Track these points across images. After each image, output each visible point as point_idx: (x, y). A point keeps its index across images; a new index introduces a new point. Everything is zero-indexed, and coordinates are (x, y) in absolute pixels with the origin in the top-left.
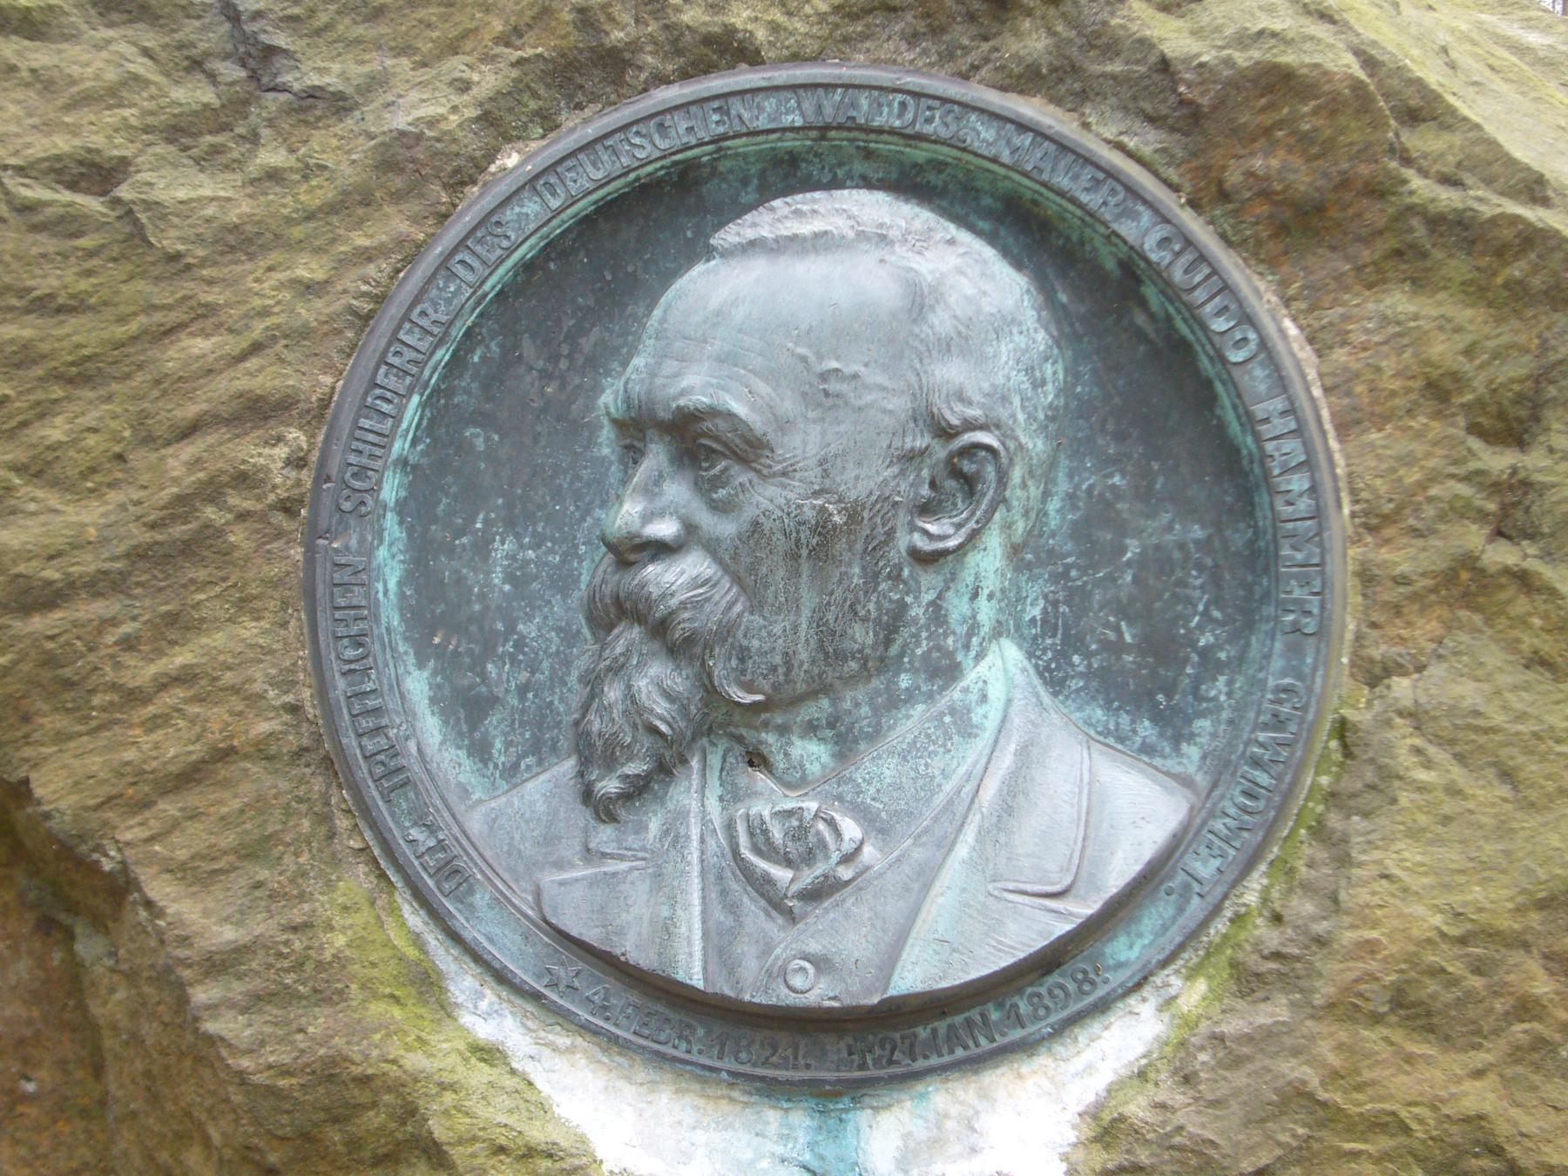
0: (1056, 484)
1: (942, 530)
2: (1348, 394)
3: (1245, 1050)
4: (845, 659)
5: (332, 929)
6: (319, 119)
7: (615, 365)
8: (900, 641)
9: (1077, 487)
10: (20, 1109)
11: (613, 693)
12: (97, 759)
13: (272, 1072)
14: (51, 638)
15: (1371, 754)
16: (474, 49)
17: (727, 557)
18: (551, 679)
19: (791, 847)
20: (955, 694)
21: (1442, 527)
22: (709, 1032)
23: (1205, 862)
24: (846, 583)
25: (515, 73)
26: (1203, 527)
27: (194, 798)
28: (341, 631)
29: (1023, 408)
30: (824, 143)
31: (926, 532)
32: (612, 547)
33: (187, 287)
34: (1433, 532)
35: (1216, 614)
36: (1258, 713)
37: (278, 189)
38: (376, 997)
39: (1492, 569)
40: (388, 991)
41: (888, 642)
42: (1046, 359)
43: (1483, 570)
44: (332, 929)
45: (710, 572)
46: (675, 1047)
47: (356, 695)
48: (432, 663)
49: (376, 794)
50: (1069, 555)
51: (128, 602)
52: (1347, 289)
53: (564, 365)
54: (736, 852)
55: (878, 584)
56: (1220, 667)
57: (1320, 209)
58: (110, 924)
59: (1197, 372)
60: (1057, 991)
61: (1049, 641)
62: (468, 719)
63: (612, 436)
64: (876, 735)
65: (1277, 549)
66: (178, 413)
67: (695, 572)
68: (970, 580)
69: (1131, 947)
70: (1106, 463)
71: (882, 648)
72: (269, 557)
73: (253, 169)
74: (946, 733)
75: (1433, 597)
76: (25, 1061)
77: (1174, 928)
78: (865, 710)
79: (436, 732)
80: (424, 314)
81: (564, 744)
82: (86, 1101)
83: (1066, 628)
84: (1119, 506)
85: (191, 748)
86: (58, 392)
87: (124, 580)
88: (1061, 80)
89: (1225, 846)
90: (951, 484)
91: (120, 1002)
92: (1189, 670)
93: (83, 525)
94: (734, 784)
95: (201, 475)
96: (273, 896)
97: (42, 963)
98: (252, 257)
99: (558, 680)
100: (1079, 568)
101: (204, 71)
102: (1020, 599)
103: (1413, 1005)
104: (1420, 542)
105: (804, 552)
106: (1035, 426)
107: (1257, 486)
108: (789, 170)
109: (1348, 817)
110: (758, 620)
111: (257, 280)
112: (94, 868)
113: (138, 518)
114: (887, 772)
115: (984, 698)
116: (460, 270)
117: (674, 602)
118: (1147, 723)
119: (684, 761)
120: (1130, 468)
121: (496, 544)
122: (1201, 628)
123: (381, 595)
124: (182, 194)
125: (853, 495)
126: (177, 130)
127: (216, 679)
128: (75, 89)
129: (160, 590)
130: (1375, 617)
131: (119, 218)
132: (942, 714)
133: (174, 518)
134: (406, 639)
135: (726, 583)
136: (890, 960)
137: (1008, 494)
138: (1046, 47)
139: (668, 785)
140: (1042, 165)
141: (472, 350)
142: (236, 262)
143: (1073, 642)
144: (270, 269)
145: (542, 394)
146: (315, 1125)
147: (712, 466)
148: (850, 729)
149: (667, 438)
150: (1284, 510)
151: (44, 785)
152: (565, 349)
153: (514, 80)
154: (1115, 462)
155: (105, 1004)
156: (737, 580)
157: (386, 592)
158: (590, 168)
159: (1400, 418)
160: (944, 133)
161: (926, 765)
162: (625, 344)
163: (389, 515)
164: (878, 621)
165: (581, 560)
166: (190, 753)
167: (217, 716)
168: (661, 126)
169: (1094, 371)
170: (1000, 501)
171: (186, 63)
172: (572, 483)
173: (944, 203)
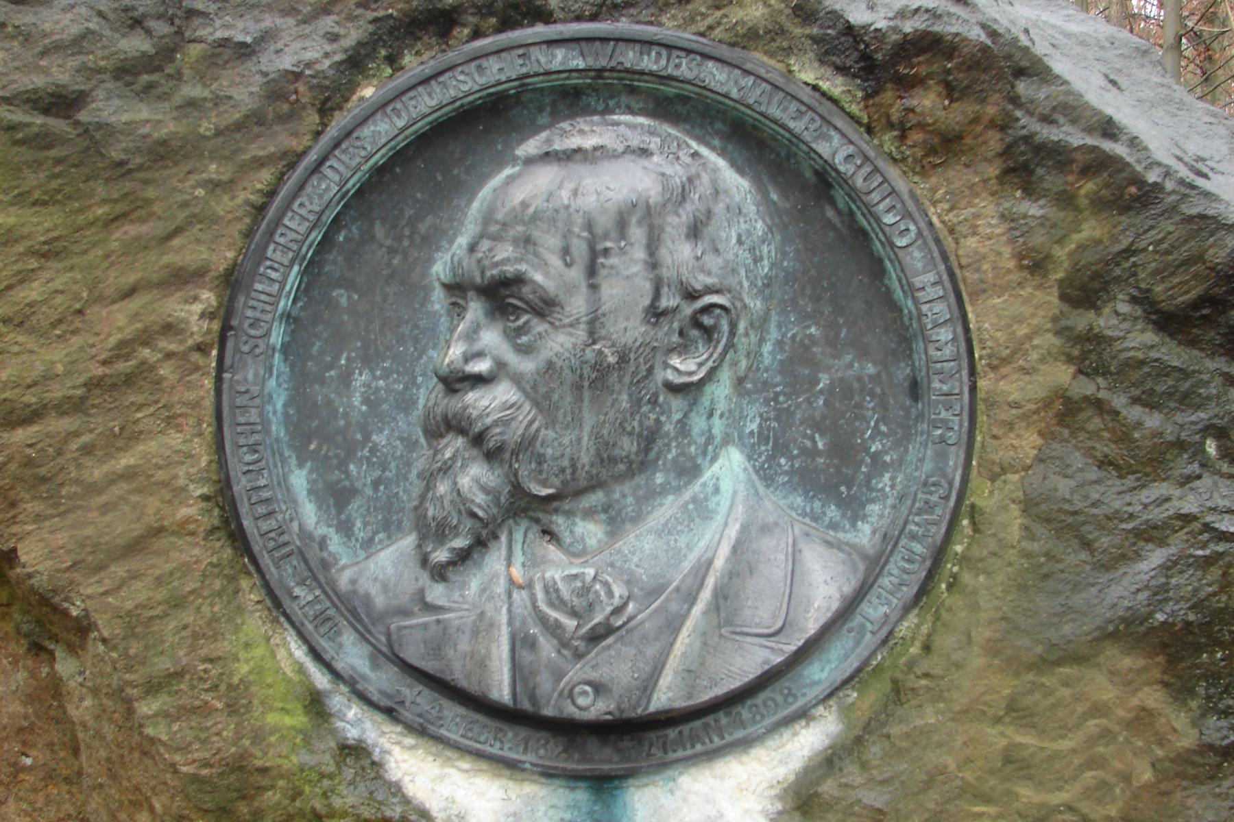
0: (768, 333)
1: (685, 366)
2: (978, 270)
3: (904, 744)
4: (616, 463)
5: (238, 660)
6: (226, 62)
7: (444, 243)
8: (656, 449)
9: (784, 335)
10: (22, 776)
11: (442, 488)
12: (66, 534)
13: (196, 764)
14: (30, 446)
15: (993, 531)
16: (341, 11)
17: (528, 387)
18: (397, 475)
19: (576, 601)
20: (696, 488)
21: (1042, 367)
22: (516, 735)
23: (875, 609)
24: (616, 407)
25: (371, 28)
26: (875, 364)
27: (134, 564)
28: (242, 441)
29: (747, 277)
30: (601, 81)
31: (676, 369)
32: (444, 380)
33: (128, 186)
34: (1035, 370)
35: (884, 428)
36: (914, 501)
37: (196, 114)
38: (271, 709)
39: (1076, 398)
40: (280, 705)
41: (647, 450)
42: (763, 242)
43: (1069, 398)
44: (238, 660)
45: (514, 398)
46: (491, 746)
47: (253, 489)
48: (309, 464)
49: (269, 562)
50: (777, 385)
51: (86, 419)
52: (977, 195)
53: (406, 243)
54: (535, 606)
55: (640, 407)
56: (886, 467)
57: (959, 137)
58: (80, 652)
59: (871, 253)
60: (769, 703)
61: (763, 448)
62: (337, 505)
63: (442, 295)
64: (637, 518)
65: (929, 382)
66: (123, 280)
67: (504, 399)
68: (707, 404)
69: (822, 670)
70: (806, 318)
71: (643, 454)
72: (189, 386)
73: (177, 100)
74: (689, 517)
75: (1035, 417)
76: (24, 743)
77: (853, 656)
78: (630, 500)
79: (312, 515)
80: (302, 205)
81: (407, 524)
82: (68, 771)
83: (776, 438)
84: (814, 349)
85: (133, 526)
86: (33, 263)
87: (83, 403)
88: (773, 40)
89: (890, 597)
90: (695, 333)
91: (87, 709)
92: (864, 469)
93: (53, 363)
94: (533, 554)
95: (139, 325)
96: (195, 636)
97: (33, 675)
98: (176, 163)
99: (402, 477)
100: (785, 395)
101: (143, 28)
102: (743, 417)
103: (1023, 710)
104: (1027, 378)
105: (586, 384)
106: (755, 291)
107: (915, 336)
108: (573, 97)
109: (978, 575)
110: (551, 434)
111: (179, 181)
112: (65, 613)
113: (93, 357)
114: (647, 546)
115: (717, 490)
116: (329, 172)
117: (489, 421)
118: (833, 507)
119: (496, 537)
120: (822, 322)
121: (356, 376)
122: (872, 438)
123: (271, 415)
124: (125, 117)
125: (623, 340)
126: (125, 71)
127: (152, 476)
128: (47, 41)
129: (110, 410)
130: (995, 431)
131: (79, 135)
132: (687, 503)
133: (118, 357)
134: (290, 447)
135: (527, 407)
136: (648, 685)
137: (735, 340)
138: (763, 15)
139: (486, 553)
140: (761, 100)
141: (338, 232)
142: (166, 167)
143: (781, 448)
144: (189, 173)
145: (389, 265)
146: (231, 801)
147: (517, 319)
148: (619, 513)
149: (483, 298)
150: (933, 352)
151: (27, 553)
152: (407, 232)
153: (371, 34)
154: (813, 317)
155: (77, 708)
156: (536, 404)
157: (275, 412)
158: (426, 98)
159: (1014, 288)
160: (689, 75)
161: (676, 540)
162: (451, 228)
163: (277, 355)
164: (640, 435)
165: (419, 388)
166: (134, 530)
167: (152, 505)
168: (479, 67)
169: (797, 252)
170: (730, 346)
171: (130, 22)
172: (412, 330)
173: (688, 127)
